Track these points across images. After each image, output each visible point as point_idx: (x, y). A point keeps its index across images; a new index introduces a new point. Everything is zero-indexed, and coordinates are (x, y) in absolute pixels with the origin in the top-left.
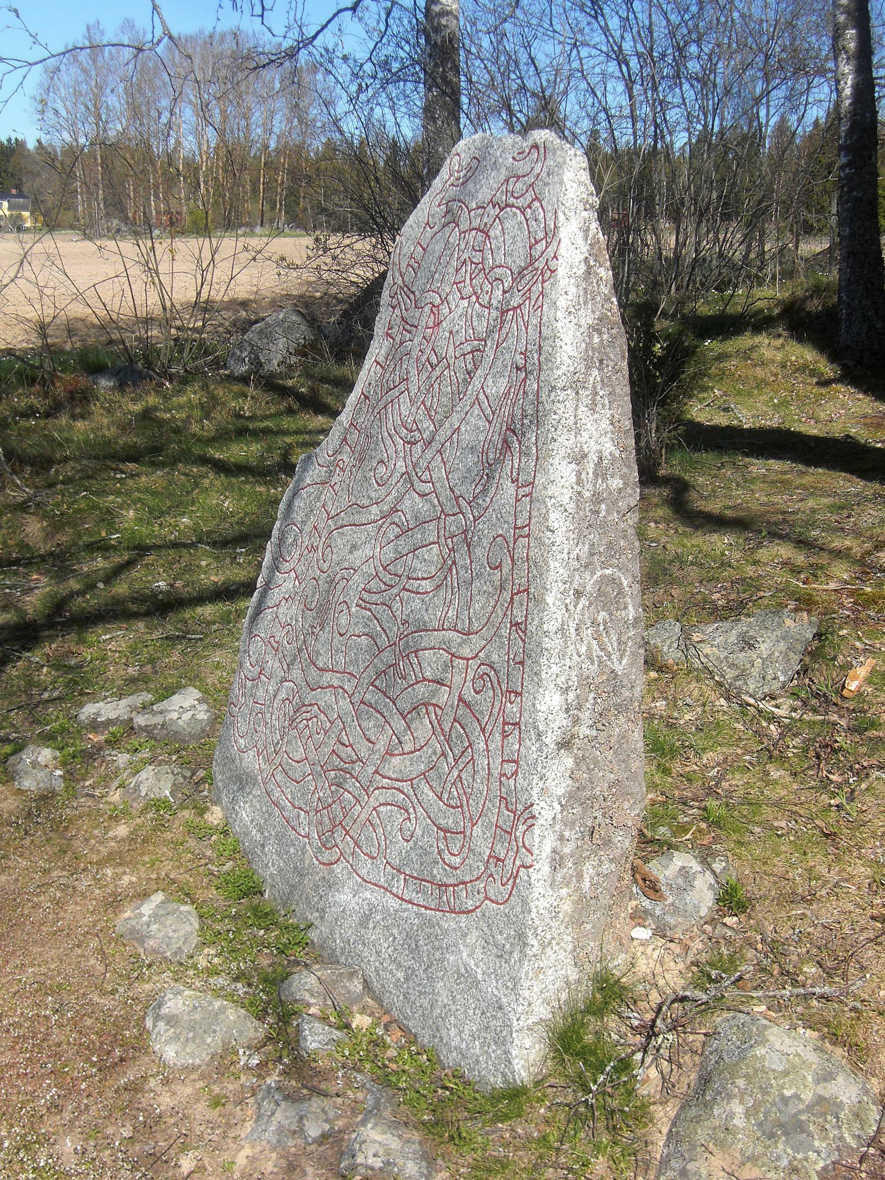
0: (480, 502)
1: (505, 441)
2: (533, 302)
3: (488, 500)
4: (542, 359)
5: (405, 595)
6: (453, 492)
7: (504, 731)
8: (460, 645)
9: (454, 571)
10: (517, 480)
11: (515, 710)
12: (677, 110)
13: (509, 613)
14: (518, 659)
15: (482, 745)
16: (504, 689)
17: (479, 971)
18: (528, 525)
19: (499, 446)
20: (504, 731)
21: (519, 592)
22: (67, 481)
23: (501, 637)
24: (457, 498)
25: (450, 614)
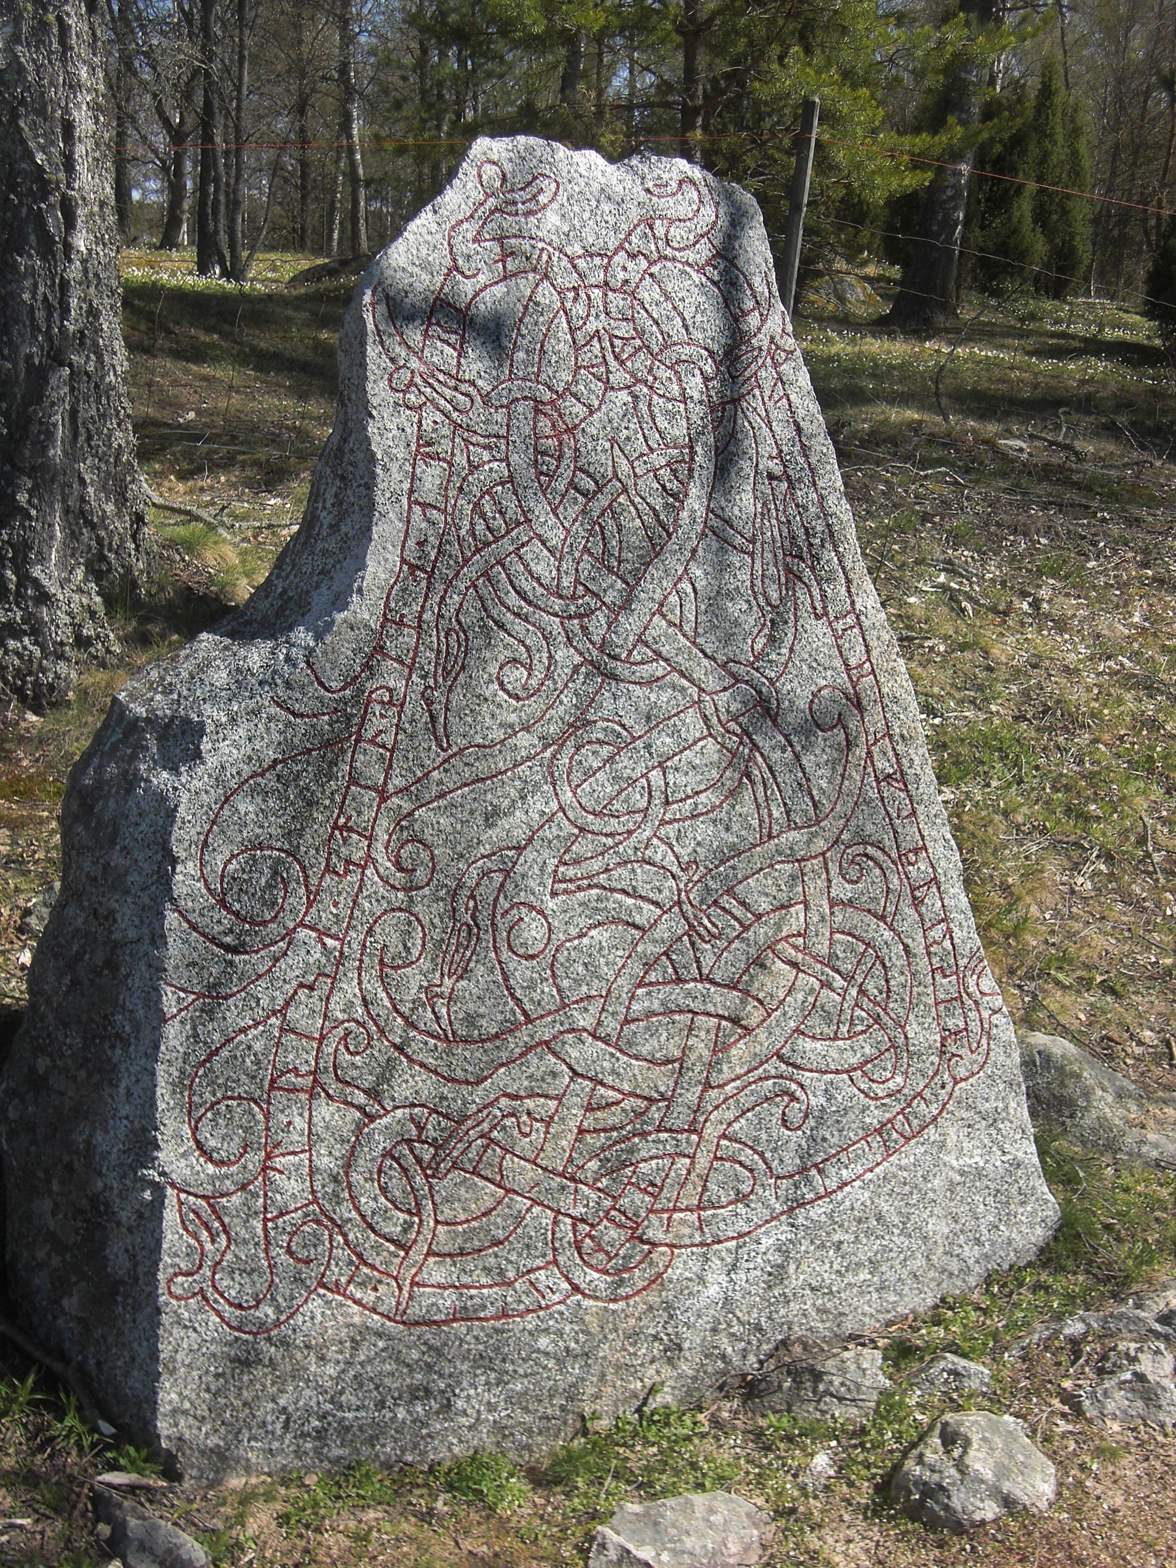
0: (773, 657)
1: (789, 570)
2: (767, 393)
3: (784, 651)
4: (813, 460)
5: (670, 831)
6: (714, 660)
7: (914, 898)
8: (809, 842)
9: (760, 759)
10: (826, 614)
11: (923, 868)
12: (593, 281)
13: (870, 770)
14: (904, 813)
15: (888, 935)
16: (894, 855)
17: (977, 1159)
18: (869, 660)
19: (783, 580)
20: (914, 898)
21: (876, 741)
22: (677, 498)
23: (868, 802)
24: (724, 666)
25: (776, 814)
